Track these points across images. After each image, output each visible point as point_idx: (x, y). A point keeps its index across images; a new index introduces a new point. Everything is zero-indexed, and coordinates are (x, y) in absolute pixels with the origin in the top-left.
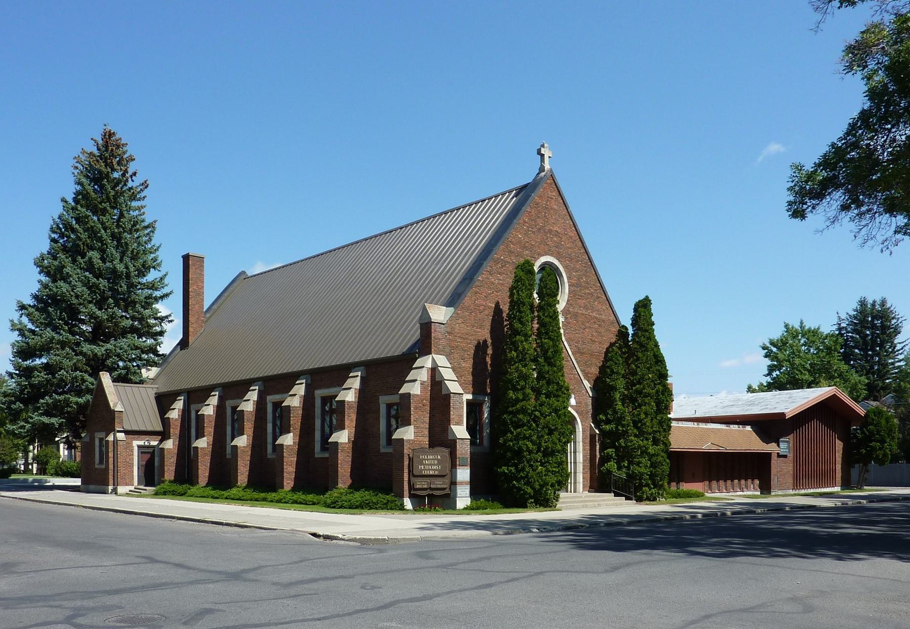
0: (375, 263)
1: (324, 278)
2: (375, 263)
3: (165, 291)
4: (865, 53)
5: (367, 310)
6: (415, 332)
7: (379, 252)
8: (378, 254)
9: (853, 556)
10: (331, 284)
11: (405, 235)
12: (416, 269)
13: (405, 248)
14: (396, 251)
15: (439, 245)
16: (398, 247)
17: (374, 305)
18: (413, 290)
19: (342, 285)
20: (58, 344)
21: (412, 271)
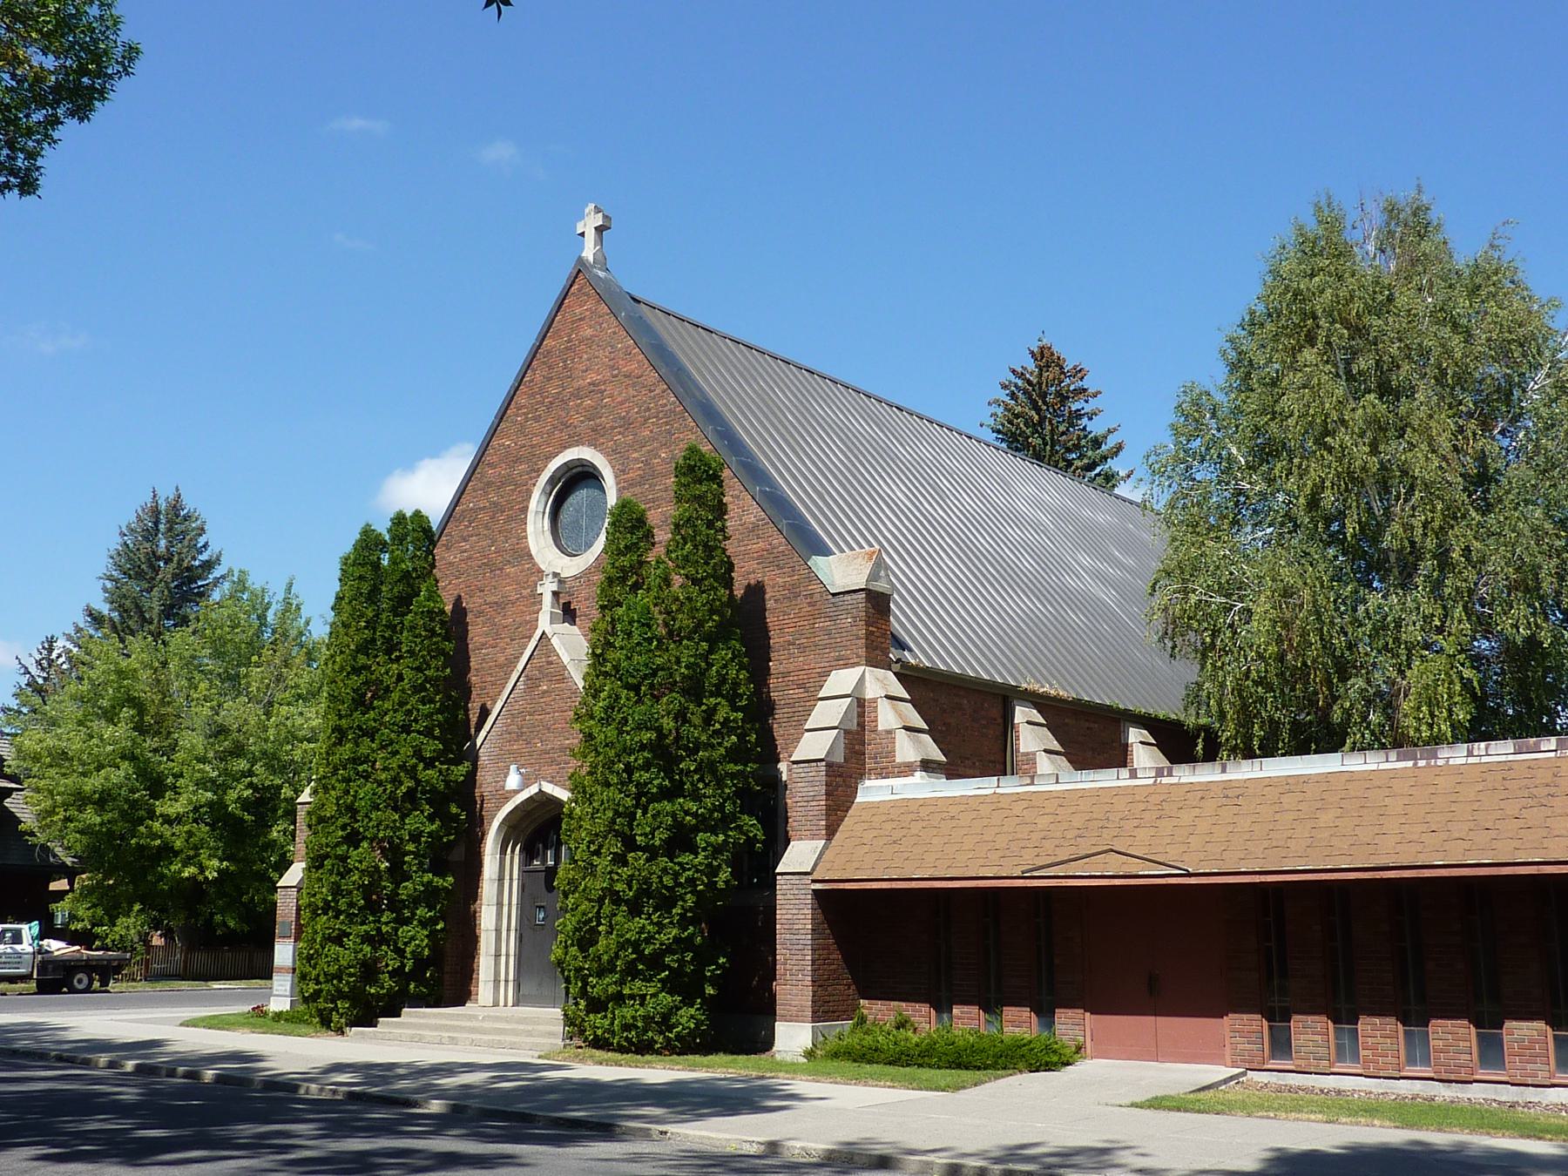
0: (802, 403)
1: (1057, 644)
2: (802, 403)
3: (1012, 378)
4: (638, 528)
5: (1048, 659)
6: (1000, 674)
7: (1039, 590)
8: (1048, 592)
9: (1554, 1146)
10: (1068, 661)
11: (764, 427)
12: (793, 432)
13: (799, 439)
14: (997, 561)
15: (852, 491)
16: (1019, 573)
17: (1058, 654)
18: (864, 457)
19: (1077, 661)
20: (720, 866)
21: (994, 558)
